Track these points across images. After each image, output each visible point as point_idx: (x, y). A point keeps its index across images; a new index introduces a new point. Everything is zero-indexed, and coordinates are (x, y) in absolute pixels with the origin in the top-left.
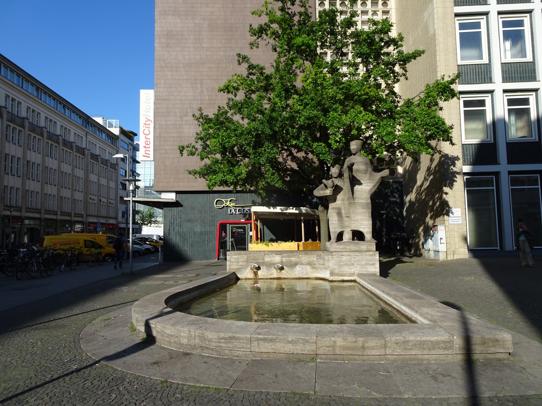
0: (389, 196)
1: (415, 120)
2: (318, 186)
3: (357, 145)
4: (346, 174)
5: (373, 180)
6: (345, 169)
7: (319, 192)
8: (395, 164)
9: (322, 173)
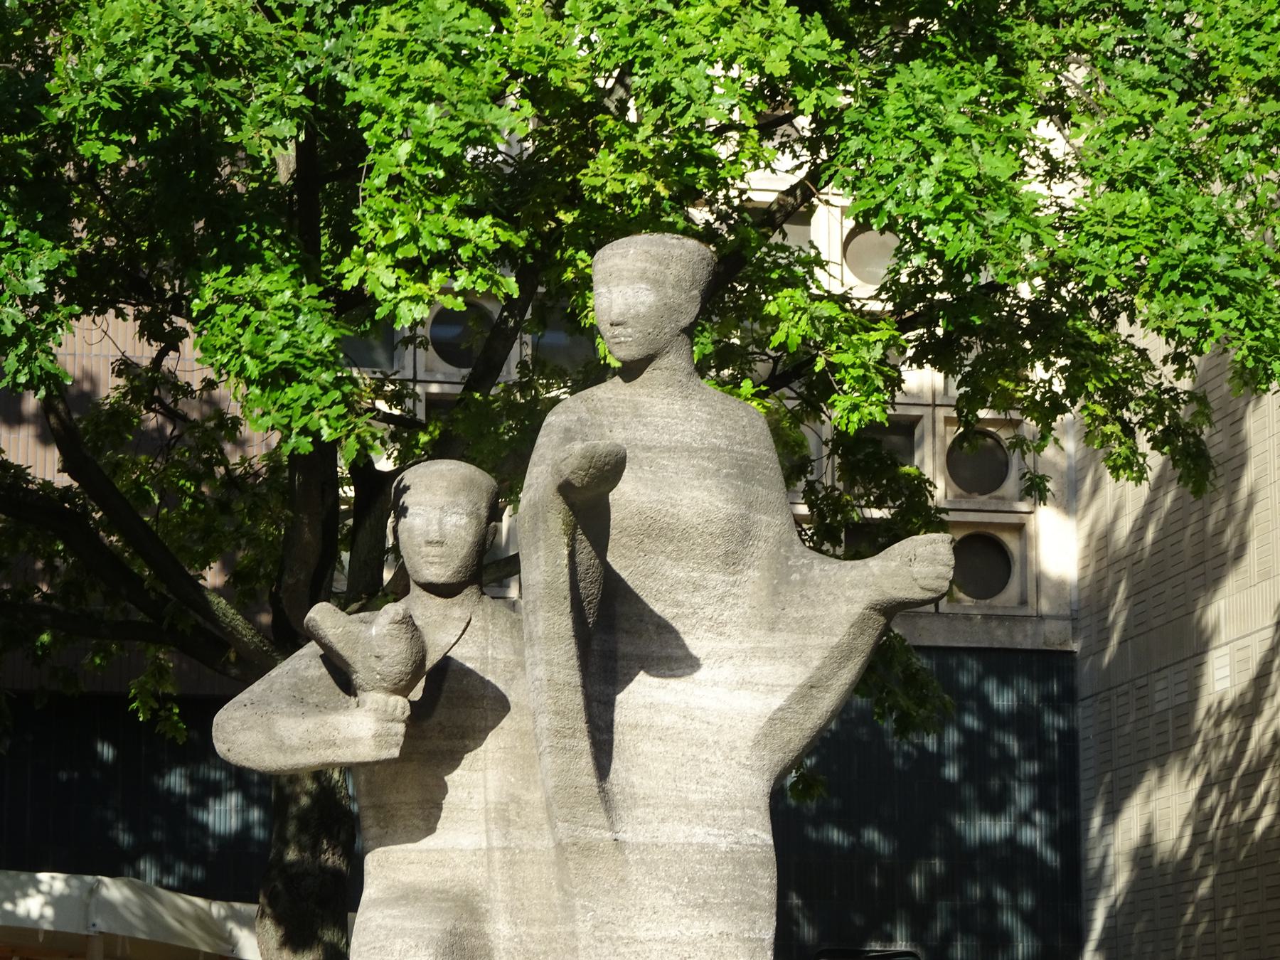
0: (950, 798)
1: (1201, 79)
2: (254, 668)
3: (657, 284)
4: (544, 564)
5: (805, 625)
6: (538, 514)
7: (277, 727)
8: (1011, 485)
9: (326, 537)
